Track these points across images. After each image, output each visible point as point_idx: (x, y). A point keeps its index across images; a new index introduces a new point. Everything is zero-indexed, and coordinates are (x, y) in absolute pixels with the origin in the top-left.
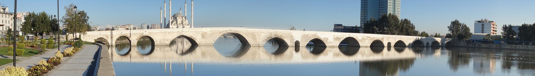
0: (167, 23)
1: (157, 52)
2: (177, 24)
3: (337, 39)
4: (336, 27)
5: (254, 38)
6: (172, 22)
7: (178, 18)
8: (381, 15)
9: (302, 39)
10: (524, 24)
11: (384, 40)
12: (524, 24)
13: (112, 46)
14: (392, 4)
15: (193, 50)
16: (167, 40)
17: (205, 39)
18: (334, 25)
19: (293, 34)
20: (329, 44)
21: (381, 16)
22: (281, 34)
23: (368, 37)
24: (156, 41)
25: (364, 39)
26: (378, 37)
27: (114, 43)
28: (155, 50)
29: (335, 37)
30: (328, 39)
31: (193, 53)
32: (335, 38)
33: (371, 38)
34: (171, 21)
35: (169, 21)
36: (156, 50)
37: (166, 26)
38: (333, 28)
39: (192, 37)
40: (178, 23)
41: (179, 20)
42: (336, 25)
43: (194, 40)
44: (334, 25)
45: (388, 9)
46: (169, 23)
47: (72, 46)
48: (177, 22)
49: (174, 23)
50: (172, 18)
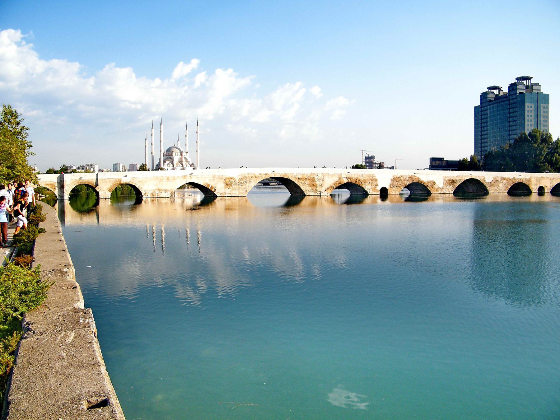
0: (156, 163)
1: (146, 207)
2: (173, 164)
3: (451, 182)
4: (434, 163)
5: (313, 186)
8: (512, 139)
9: (392, 184)
10: (466, 158)
11: (533, 183)
12: (466, 158)
14: (532, 118)
15: (211, 204)
16: (166, 191)
17: (231, 190)
18: (430, 158)
19: (377, 177)
20: (436, 191)
21: (513, 140)
22: (356, 176)
23: (504, 178)
24: (145, 194)
25: (496, 182)
26: (520, 177)
27: (67, 196)
28: (143, 202)
29: (447, 179)
30: (434, 183)
31: (210, 208)
32: (447, 181)
33: (509, 180)
35: (160, 159)
36: (145, 202)
37: (155, 167)
38: (428, 165)
39: (209, 185)
41: (176, 159)
42: (433, 160)
43: (213, 190)
44: (430, 158)
45: (526, 128)
46: (160, 162)
47: (30, 43)
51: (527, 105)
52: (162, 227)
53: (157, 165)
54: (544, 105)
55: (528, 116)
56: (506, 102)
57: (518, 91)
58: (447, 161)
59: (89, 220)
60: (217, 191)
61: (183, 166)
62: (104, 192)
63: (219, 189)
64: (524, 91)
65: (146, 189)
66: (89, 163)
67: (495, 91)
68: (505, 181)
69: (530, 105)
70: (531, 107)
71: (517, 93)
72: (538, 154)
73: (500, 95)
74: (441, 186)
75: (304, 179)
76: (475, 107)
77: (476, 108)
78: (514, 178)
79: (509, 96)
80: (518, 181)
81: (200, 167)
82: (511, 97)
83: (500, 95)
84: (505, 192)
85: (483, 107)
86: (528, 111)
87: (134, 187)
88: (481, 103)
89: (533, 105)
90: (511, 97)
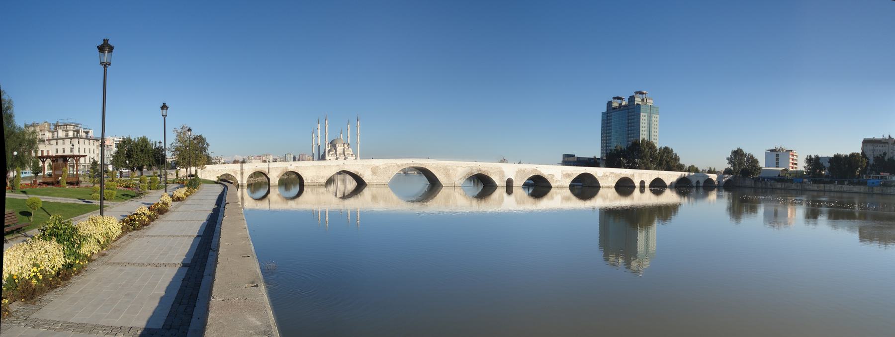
0: (321, 153)
1: (307, 195)
3: (568, 175)
4: (566, 159)
6: (329, 152)
7: (337, 145)
13: (242, 186)
15: (360, 192)
16: (323, 178)
18: (563, 155)
23: (612, 173)
24: (306, 179)
27: (245, 182)
29: (564, 173)
32: (564, 175)
33: (616, 175)
34: (327, 149)
35: (325, 149)
38: (561, 159)
40: (338, 153)
41: (340, 149)
46: (325, 153)
48: (336, 151)
49: (331, 153)
50: (330, 145)
51: (642, 114)
52: (326, 211)
53: (323, 155)
54: (655, 115)
55: (642, 134)
56: (627, 111)
57: (636, 103)
58: (577, 157)
59: (263, 205)
60: (365, 178)
61: (345, 156)
62: (274, 178)
63: (367, 177)
64: (640, 103)
65: (307, 177)
66: (265, 154)
67: (619, 101)
68: (613, 175)
69: (644, 114)
70: (645, 116)
71: (634, 104)
72: (656, 217)
73: (623, 104)
74: (559, 179)
75: (435, 168)
76: (602, 113)
77: (603, 113)
78: (621, 173)
79: (629, 105)
80: (624, 176)
81: (360, 156)
82: (630, 107)
83: (623, 104)
84: (606, 190)
85: (609, 113)
86: (643, 123)
87: (298, 174)
88: (607, 110)
89: (646, 114)
90: (630, 107)
